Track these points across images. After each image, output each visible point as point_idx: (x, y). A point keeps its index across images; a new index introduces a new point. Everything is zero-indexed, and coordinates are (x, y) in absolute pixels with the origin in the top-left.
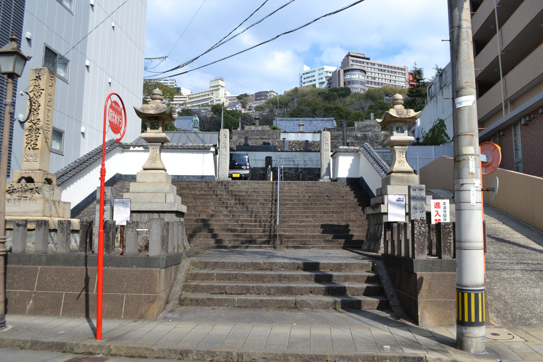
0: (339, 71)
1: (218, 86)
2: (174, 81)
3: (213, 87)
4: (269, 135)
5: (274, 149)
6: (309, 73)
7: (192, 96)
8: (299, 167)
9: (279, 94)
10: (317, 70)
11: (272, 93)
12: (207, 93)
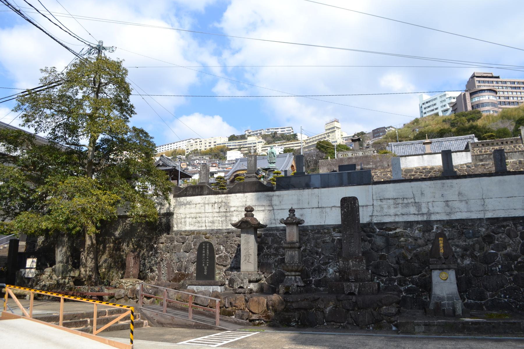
0: (464, 95)
1: (334, 128)
2: (291, 129)
3: (329, 129)
4: (375, 163)
5: (364, 178)
6: (429, 102)
7: (309, 141)
8: (433, 218)
9: (398, 127)
10: (438, 98)
11: (391, 128)
12: (323, 136)
